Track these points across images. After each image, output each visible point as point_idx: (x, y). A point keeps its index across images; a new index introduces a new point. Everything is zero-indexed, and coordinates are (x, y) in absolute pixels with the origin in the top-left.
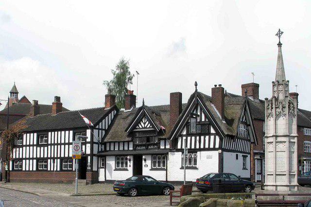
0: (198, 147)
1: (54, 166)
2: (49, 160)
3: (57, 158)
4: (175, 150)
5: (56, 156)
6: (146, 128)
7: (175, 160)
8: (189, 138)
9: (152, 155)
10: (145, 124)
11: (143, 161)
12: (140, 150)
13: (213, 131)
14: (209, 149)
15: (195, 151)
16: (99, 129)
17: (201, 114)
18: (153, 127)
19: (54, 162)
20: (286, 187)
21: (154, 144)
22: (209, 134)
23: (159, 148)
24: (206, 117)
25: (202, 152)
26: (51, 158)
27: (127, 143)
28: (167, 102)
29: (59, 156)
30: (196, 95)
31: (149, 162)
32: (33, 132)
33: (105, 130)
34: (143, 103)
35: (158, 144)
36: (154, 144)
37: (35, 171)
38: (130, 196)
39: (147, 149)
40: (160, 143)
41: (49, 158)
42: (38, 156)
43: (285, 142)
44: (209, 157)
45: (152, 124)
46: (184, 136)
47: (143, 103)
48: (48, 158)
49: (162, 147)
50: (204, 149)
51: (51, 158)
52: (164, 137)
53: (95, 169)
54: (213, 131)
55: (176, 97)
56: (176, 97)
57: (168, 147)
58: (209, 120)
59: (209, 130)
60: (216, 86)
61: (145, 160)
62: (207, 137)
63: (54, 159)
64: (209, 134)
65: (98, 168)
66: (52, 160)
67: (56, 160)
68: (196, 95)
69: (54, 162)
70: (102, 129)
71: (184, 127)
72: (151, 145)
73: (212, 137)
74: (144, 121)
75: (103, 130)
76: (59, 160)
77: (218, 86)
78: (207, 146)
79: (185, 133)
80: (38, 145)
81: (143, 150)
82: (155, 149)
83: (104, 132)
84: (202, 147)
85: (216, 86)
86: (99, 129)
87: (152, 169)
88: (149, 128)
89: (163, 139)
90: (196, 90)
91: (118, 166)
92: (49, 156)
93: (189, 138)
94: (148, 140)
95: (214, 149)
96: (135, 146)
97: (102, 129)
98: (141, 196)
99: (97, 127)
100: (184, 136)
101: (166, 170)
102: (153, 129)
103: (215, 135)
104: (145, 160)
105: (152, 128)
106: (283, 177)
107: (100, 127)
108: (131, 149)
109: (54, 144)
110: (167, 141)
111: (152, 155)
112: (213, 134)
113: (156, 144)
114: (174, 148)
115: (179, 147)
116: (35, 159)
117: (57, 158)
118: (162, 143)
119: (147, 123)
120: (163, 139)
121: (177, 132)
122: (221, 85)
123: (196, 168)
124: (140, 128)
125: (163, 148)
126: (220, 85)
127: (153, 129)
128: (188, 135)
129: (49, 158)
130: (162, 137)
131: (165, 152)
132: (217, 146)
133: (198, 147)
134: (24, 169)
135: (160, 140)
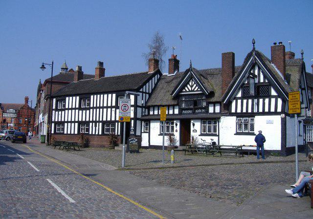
1: (96, 130)
2: (91, 124)
3: (99, 122)
5: (98, 120)
6: (193, 91)
7: (228, 126)
8: (245, 101)
10: (192, 87)
13: (273, 93)
14: (269, 113)
15: (253, 115)
16: (143, 92)
17: (259, 74)
19: (96, 126)
23: (207, 111)
24: (265, 77)
26: (93, 122)
29: (101, 120)
30: (254, 53)
32: (76, 95)
33: (149, 93)
36: (202, 108)
37: (76, 135)
41: (91, 122)
42: (56, 120)
44: (269, 122)
45: (200, 87)
46: (239, 98)
48: (89, 122)
50: (264, 113)
51: (93, 122)
53: (138, 133)
54: (273, 93)
56: (229, 58)
63: (96, 122)
64: (270, 97)
65: (141, 133)
66: (94, 124)
67: (98, 124)
68: (254, 53)
69: (96, 126)
70: (146, 93)
73: (273, 100)
75: (147, 93)
76: (101, 124)
77: (278, 44)
78: (267, 110)
79: (239, 95)
80: (80, 108)
81: (189, 114)
83: (147, 95)
85: (275, 44)
86: (143, 92)
88: (197, 91)
92: (91, 120)
94: (195, 103)
95: (276, 113)
96: (181, 110)
97: (146, 93)
99: (141, 90)
101: (218, 136)
105: (201, 91)
107: (144, 91)
108: (177, 111)
109: (96, 108)
112: (274, 97)
114: (226, 109)
116: (76, 122)
117: (99, 122)
122: (281, 43)
124: (186, 91)
127: (201, 92)
128: (242, 98)
129: (91, 122)
132: (279, 110)
134: (65, 132)
135: (209, 103)
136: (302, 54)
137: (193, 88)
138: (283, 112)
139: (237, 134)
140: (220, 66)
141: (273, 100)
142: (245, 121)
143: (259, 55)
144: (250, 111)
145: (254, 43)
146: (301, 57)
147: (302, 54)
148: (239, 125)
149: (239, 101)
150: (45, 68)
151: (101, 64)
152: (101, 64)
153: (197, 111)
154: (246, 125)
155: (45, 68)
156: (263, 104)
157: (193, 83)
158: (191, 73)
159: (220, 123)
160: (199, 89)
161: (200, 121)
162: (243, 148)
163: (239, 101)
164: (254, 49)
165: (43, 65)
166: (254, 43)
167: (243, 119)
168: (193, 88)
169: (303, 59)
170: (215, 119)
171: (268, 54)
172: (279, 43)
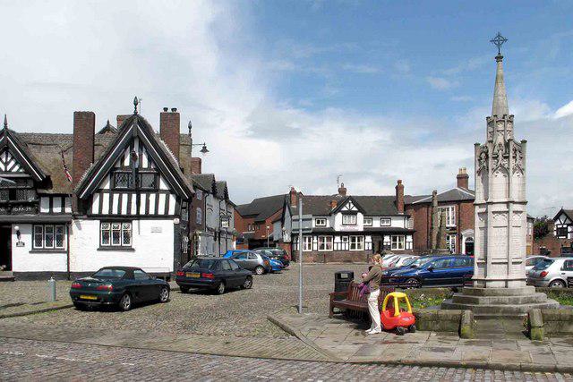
0: (134, 212)
4: (85, 217)
7: (85, 235)
8: (116, 196)
9: (33, 223)
11: (14, 237)
12: (20, 212)
13: (163, 186)
14: (156, 217)
15: (128, 219)
17: (141, 155)
18: (27, 171)
20: (520, 282)
21: (26, 204)
22: (157, 191)
23: (38, 211)
24: (150, 160)
25: (141, 221)
27: (48, 199)
28: (68, 128)
30: (136, 121)
31: (27, 238)
34: (6, 124)
35: (35, 206)
36: (26, 204)
38: (122, 310)
39: (9, 212)
40: (38, 203)
43: (521, 212)
44: (156, 231)
45: (23, 165)
46: (107, 191)
47: (6, 124)
49: (45, 210)
50: (147, 217)
52: (51, 191)
54: (163, 186)
55: (84, 120)
56: (84, 120)
57: (68, 210)
58: (27, 171)
59: (156, 183)
60: (166, 109)
61: (18, 233)
62: (152, 197)
64: (157, 191)
68: (136, 121)
71: (107, 175)
72: (18, 205)
73: (162, 197)
74: (4, 160)
78: (152, 212)
79: (107, 186)
82: (29, 212)
84: (142, 212)
85: (166, 109)
87: (33, 251)
88: (17, 172)
89: (45, 195)
90: (136, 113)
91: (39, 244)
93: (116, 196)
94: (13, 193)
95: (166, 217)
98: (137, 307)
100: (107, 191)
102: (28, 175)
103: (168, 193)
104: (18, 233)
105: (25, 173)
106: (519, 265)
110: (54, 199)
111: (33, 223)
112: (164, 191)
113: (32, 204)
114: (84, 208)
115: (95, 210)
118: (44, 202)
119: (13, 163)
120: (45, 195)
121: (93, 185)
123: (131, 249)
125: (48, 211)
126: (174, 109)
128: (112, 191)
130: (47, 192)
131: (63, 218)
132: (172, 212)
133: (134, 212)
135: (40, 196)
136: (190, 127)
137: (9, 168)
138: (176, 215)
139: (101, 249)
140: (71, 132)
141: (162, 197)
142: (116, 230)
143: (143, 124)
144: (124, 212)
145: (136, 104)
146: (188, 133)
147: (190, 127)
148: (105, 236)
149: (106, 196)
150: (207, 151)
151: (399, 182)
152: (399, 182)
153: (15, 209)
154: (116, 236)
155: (207, 151)
156: (150, 202)
157: (9, 159)
158: (5, 138)
159: (71, 236)
160: (21, 171)
161: (31, 226)
162: (198, 209)
163: (106, 196)
164: (136, 113)
165: (205, 148)
166: (136, 104)
167: (111, 227)
168: (8, 168)
169: (190, 135)
170: (63, 223)
171: (156, 127)
172: (172, 109)
